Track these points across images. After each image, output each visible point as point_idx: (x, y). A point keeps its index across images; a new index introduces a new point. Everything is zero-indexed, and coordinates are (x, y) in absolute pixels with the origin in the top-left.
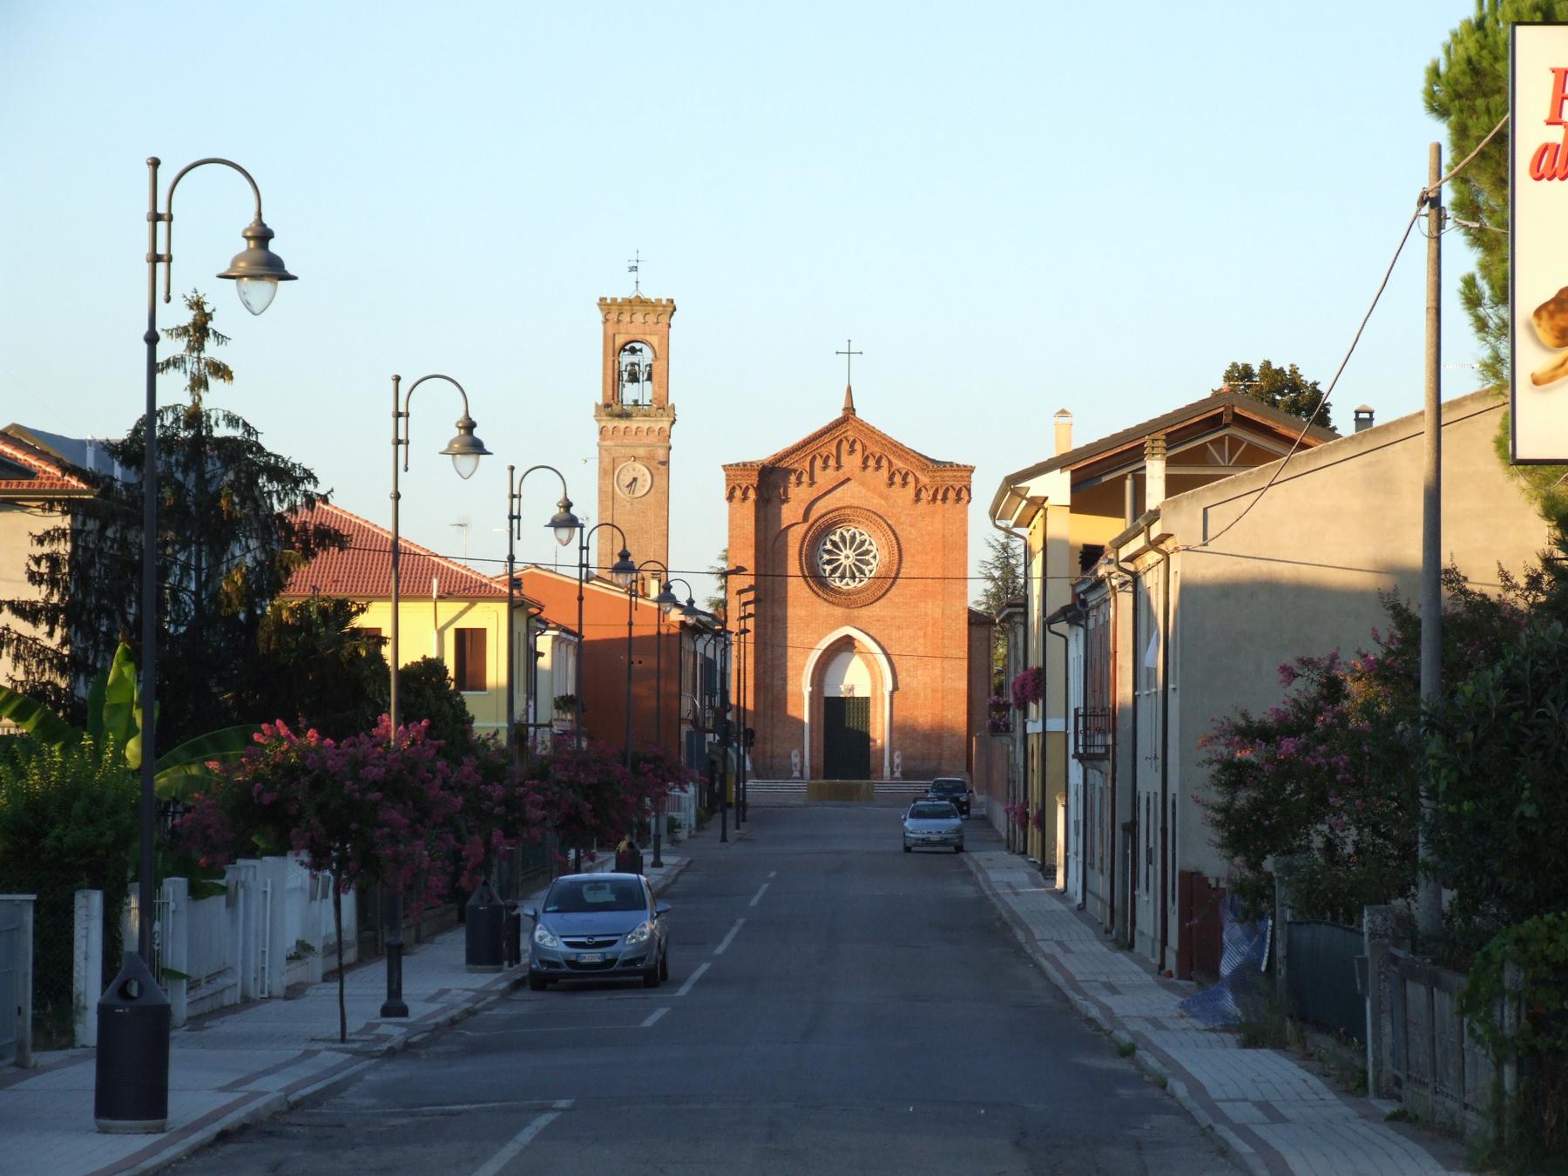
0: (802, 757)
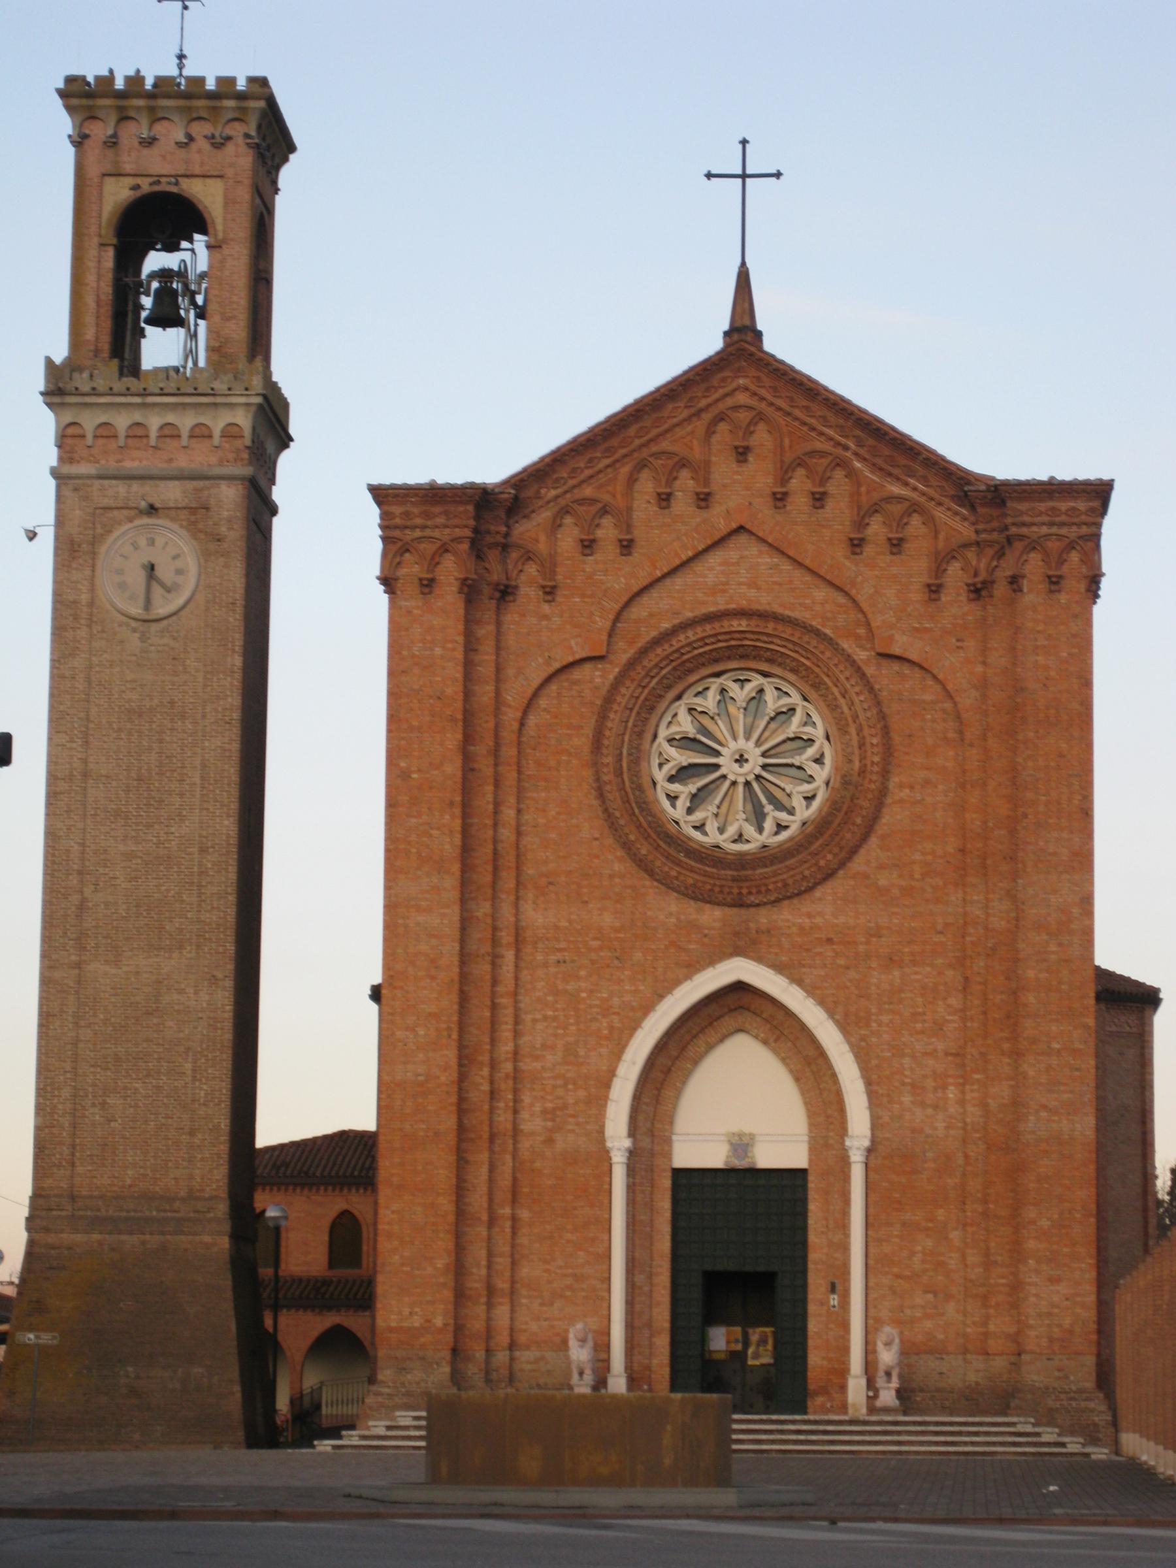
0: (602, 1347)
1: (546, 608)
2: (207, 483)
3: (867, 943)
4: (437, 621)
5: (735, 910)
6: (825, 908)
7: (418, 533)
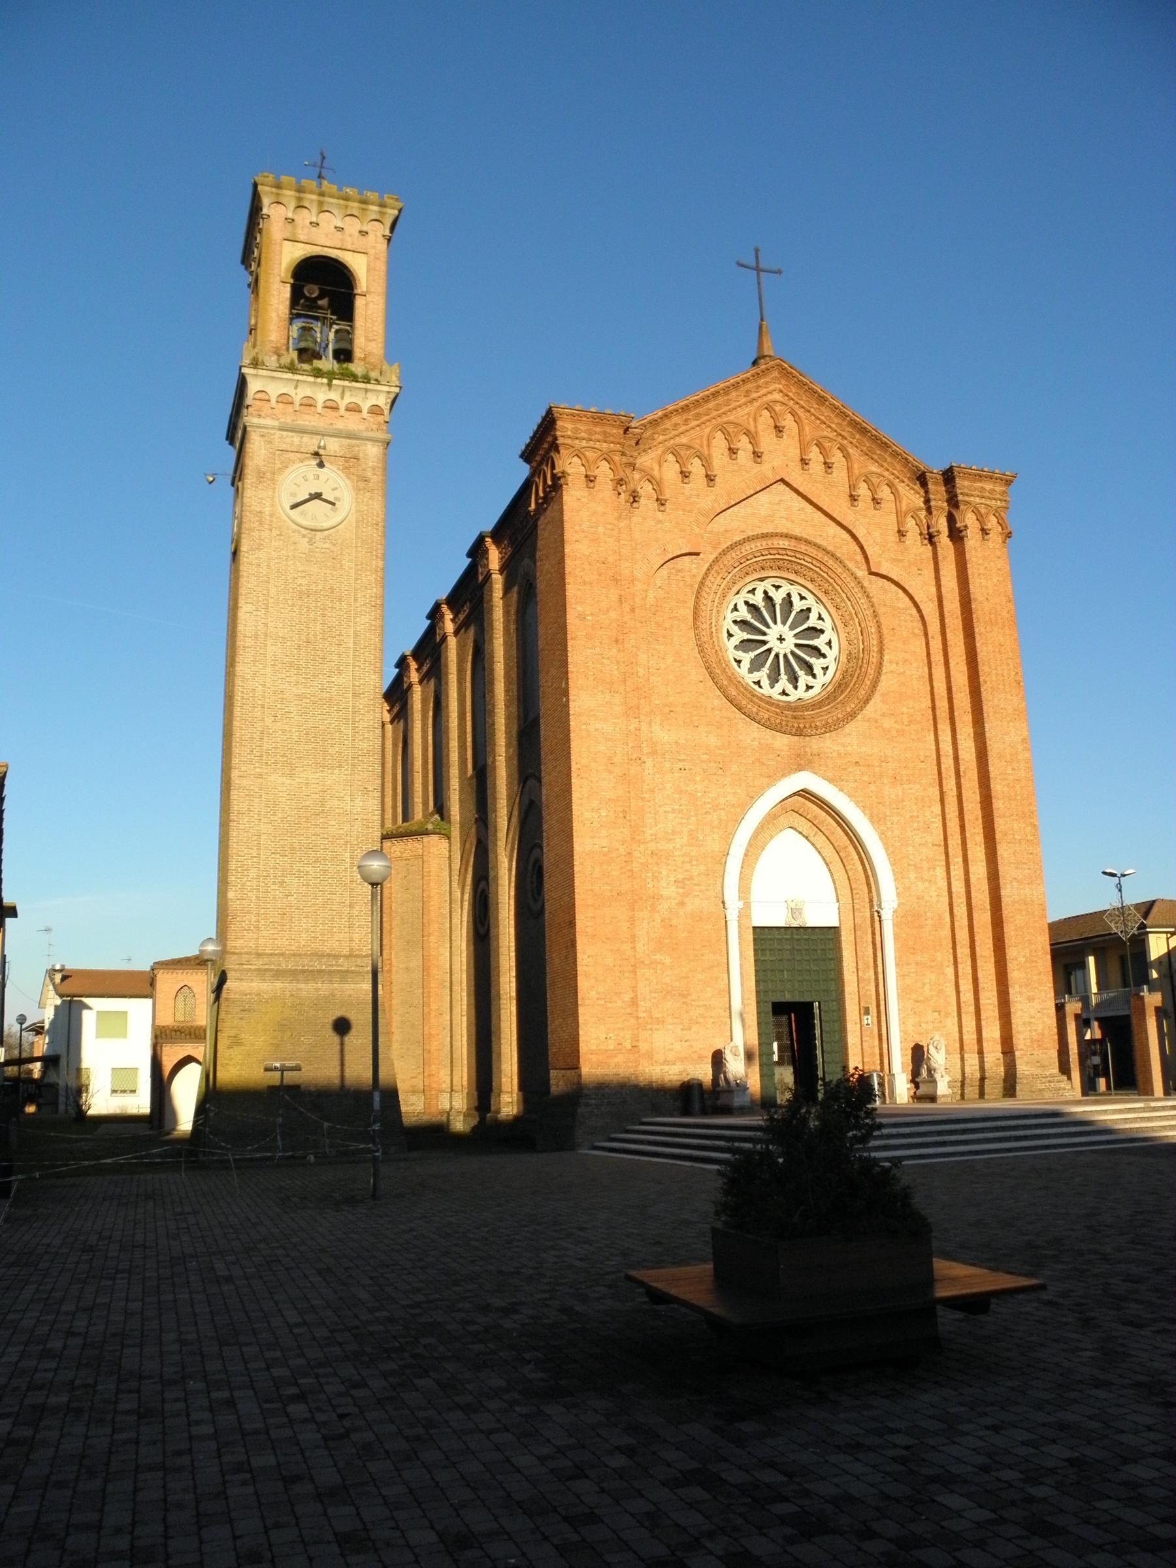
1: (660, 515)
2: (357, 442)
3: (880, 766)
4: (600, 509)
5: (797, 738)
6: (851, 740)
7: (584, 443)
